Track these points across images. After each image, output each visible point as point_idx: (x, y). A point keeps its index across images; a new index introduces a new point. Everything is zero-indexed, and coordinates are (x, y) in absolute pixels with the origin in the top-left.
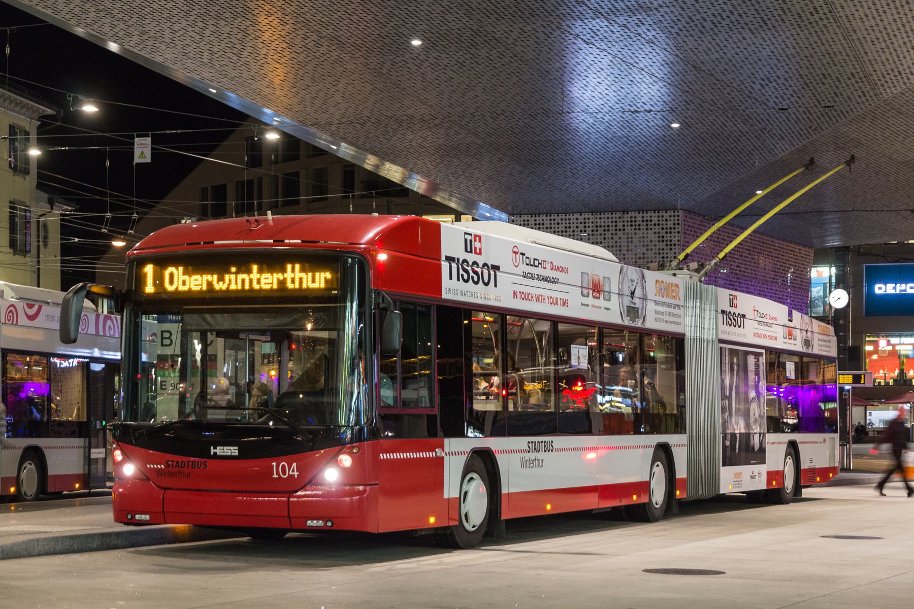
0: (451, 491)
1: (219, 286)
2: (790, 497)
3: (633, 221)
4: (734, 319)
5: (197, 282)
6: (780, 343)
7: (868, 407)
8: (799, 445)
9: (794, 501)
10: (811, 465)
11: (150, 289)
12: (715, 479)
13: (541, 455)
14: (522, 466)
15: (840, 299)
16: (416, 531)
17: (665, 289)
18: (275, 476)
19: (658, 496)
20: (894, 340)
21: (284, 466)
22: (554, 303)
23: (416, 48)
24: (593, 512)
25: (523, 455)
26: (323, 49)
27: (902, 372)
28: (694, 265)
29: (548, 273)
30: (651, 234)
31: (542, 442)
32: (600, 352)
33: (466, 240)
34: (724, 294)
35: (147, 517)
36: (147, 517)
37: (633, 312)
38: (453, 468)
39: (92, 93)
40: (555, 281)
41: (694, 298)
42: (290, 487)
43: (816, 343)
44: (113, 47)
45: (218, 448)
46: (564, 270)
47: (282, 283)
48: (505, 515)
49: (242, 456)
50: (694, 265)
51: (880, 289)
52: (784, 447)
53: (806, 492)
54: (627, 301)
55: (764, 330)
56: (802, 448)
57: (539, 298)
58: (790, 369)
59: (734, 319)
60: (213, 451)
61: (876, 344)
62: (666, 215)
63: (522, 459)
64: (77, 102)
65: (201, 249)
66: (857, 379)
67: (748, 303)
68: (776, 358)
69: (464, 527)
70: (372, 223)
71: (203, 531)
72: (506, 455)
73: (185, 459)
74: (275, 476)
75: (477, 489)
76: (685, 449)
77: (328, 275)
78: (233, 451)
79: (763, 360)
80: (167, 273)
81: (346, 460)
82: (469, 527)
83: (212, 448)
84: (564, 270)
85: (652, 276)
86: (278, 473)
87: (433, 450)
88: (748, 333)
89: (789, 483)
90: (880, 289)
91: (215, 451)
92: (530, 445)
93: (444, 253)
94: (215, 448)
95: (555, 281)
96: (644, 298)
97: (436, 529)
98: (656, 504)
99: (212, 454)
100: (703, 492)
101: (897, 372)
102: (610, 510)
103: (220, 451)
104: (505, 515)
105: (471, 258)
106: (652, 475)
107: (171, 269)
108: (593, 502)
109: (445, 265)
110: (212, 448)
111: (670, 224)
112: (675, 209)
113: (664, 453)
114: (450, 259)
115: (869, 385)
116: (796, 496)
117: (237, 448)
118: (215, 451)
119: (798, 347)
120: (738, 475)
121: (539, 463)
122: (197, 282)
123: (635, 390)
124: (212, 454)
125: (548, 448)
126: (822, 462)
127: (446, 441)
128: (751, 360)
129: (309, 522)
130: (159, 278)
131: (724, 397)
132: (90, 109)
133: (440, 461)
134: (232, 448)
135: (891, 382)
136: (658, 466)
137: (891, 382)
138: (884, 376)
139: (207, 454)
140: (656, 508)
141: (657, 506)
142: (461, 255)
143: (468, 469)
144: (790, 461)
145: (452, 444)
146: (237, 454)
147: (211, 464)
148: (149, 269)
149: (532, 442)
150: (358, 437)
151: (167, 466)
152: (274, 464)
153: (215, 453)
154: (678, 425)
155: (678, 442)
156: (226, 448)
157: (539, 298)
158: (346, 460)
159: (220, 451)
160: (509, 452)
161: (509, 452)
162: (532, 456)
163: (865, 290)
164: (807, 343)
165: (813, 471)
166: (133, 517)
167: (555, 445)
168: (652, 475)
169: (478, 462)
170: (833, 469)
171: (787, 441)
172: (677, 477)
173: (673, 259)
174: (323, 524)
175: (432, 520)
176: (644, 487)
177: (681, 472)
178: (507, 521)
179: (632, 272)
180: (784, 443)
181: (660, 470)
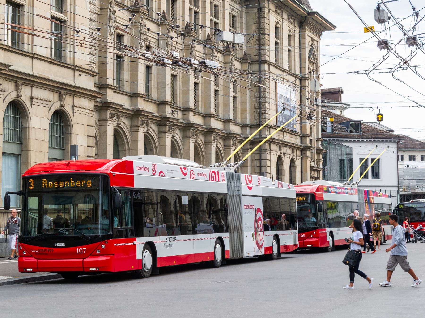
0: (139, 257)
8: (155, 243)
10: (285, 244)
13: (171, 243)
14: (165, 247)
18: (78, 253)
19: (219, 256)
21: (81, 249)
25: (164, 243)
35: (32, 270)
36: (32, 270)
38: (140, 248)
48: (158, 266)
49: (66, 246)
60: (55, 245)
65: (49, 173)
69: (143, 269)
72: (159, 243)
73: (46, 248)
74: (78, 253)
75: (148, 254)
76: (229, 239)
78: (63, 245)
86: (79, 252)
87: (132, 242)
94: (56, 244)
97: (134, 271)
100: (237, 256)
103: (58, 245)
104: (158, 266)
113: (220, 241)
116: (279, 257)
121: (171, 246)
123: (318, 164)
125: (174, 240)
127: (137, 238)
129: (91, 269)
133: (135, 246)
134: (62, 244)
139: (54, 246)
145: (139, 240)
151: (39, 251)
152: (77, 249)
153: (56, 246)
155: (226, 236)
159: (58, 245)
162: (168, 243)
166: (26, 270)
167: (341, 230)
169: (148, 247)
171: (329, 231)
172: (226, 250)
175: (133, 267)
176: (214, 254)
177: (227, 248)
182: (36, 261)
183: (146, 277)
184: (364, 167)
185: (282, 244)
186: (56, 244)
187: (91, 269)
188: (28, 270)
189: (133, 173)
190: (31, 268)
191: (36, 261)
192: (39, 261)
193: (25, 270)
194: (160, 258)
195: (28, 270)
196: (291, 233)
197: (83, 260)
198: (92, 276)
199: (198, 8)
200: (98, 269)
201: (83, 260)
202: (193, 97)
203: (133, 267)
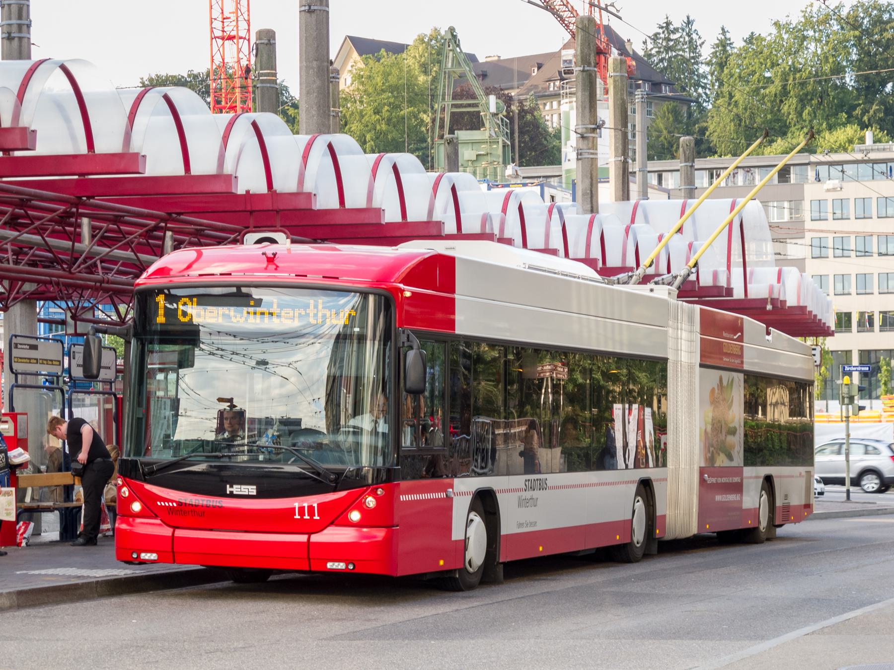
2: (640, 553)
8: (497, 495)
9: (768, 539)
13: (536, 494)
14: (519, 505)
16: (579, 552)
19: (639, 536)
24: (579, 555)
25: (519, 494)
31: (537, 480)
32: (506, 356)
38: (461, 506)
45: (235, 486)
48: (504, 558)
52: (633, 488)
56: (776, 482)
60: (229, 490)
63: (519, 498)
74: (297, 517)
82: (471, 570)
83: (228, 486)
91: (231, 489)
92: (527, 483)
94: (231, 486)
98: (638, 543)
99: (228, 492)
102: (594, 552)
110: (228, 486)
117: (255, 487)
118: (231, 489)
124: (228, 492)
127: (456, 481)
133: (449, 499)
134: (250, 487)
136: (638, 501)
140: (468, 572)
141: (638, 545)
143: (472, 508)
144: (640, 505)
146: (255, 493)
149: (529, 480)
153: (231, 492)
156: (243, 487)
160: (508, 491)
161: (508, 491)
162: (528, 494)
166: (139, 556)
167: (549, 483)
171: (637, 479)
172: (657, 514)
173: (254, 83)
174: (344, 567)
175: (442, 563)
176: (628, 525)
178: (505, 564)
180: (632, 482)
182: (167, 531)
183: (471, 587)
184: (871, 324)
185: (779, 502)
186: (231, 486)
187: (330, 565)
188: (145, 556)
189: (453, 291)
190: (152, 551)
191: (167, 531)
192: (180, 533)
193: (135, 556)
194: (507, 535)
195: (145, 556)
196: (800, 474)
197: (309, 539)
198: (305, 577)
199: (115, 273)
200: (351, 567)
201: (309, 539)
202: (205, 293)
203: (442, 563)
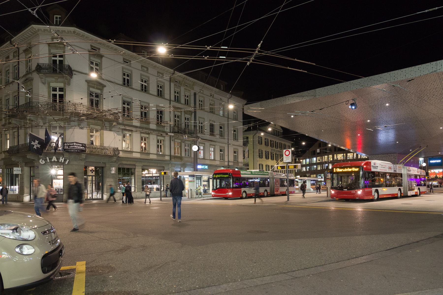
0: (373, 194)
1: (344, 171)
3: (389, 155)
4: (409, 171)
5: (341, 170)
6: (417, 174)
7: (338, 155)
11: (335, 171)
12: (407, 193)
15: (424, 165)
17: (400, 167)
19: (399, 195)
20: (434, 170)
22: (385, 170)
23: (359, 134)
26: (327, 127)
27: (436, 175)
28: (402, 163)
29: (384, 167)
30: (392, 157)
33: (175, 96)
34: (408, 167)
37: (395, 171)
39: (304, 141)
40: (385, 168)
41: (403, 168)
42: (354, 194)
43: (422, 173)
44: (307, 135)
46: (386, 166)
47: (352, 170)
50: (402, 163)
51: (431, 162)
53: (421, 195)
54: (394, 169)
55: (414, 172)
57: (383, 170)
58: (418, 177)
59: (409, 171)
61: (431, 171)
62: (395, 154)
64: (302, 143)
66: (428, 178)
67: (412, 168)
68: (416, 176)
70: (363, 162)
71: (339, 200)
75: (376, 194)
77: (358, 169)
79: (414, 176)
80: (337, 169)
81: (361, 191)
84: (386, 166)
85: (398, 165)
88: (412, 173)
89: (418, 194)
90: (431, 162)
93: (372, 165)
95: (385, 168)
96: (396, 169)
100: (406, 195)
101: (435, 176)
103: (345, 190)
105: (375, 166)
106: (398, 192)
107: (337, 169)
108: (390, 196)
109: (372, 167)
111: (395, 156)
112: (396, 153)
114: (372, 166)
115: (431, 178)
119: (419, 174)
120: (410, 192)
122: (341, 170)
126: (424, 191)
128: (412, 176)
130: (336, 170)
131: (408, 182)
132: (304, 143)
135: (434, 177)
137: (434, 177)
138: (432, 176)
142: (373, 165)
147: (344, 191)
148: (335, 169)
150: (363, 188)
154: (401, 186)
157: (383, 170)
158: (361, 191)
163: (428, 162)
164: (421, 173)
165: (423, 192)
168: (398, 192)
169: (376, 191)
170: (425, 192)
176: (397, 194)
177: (402, 192)
179: (395, 165)
181: (399, 192)
